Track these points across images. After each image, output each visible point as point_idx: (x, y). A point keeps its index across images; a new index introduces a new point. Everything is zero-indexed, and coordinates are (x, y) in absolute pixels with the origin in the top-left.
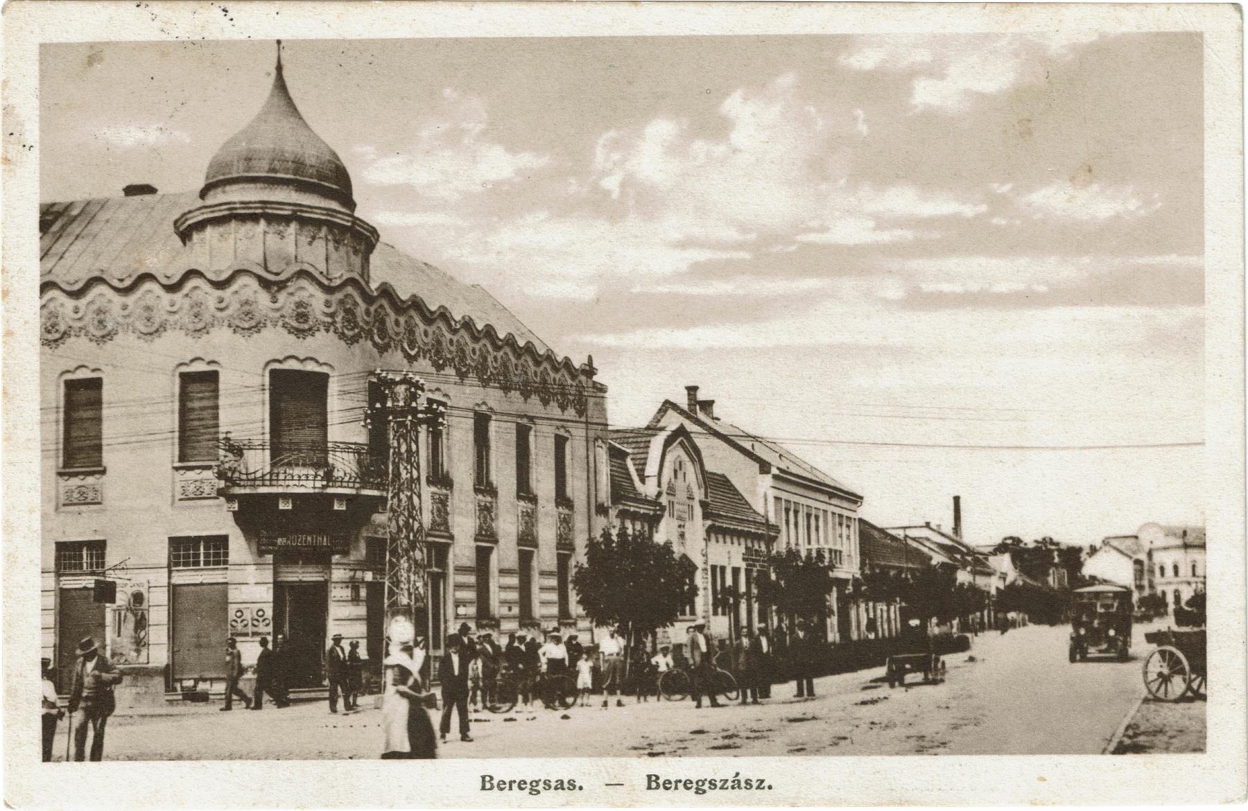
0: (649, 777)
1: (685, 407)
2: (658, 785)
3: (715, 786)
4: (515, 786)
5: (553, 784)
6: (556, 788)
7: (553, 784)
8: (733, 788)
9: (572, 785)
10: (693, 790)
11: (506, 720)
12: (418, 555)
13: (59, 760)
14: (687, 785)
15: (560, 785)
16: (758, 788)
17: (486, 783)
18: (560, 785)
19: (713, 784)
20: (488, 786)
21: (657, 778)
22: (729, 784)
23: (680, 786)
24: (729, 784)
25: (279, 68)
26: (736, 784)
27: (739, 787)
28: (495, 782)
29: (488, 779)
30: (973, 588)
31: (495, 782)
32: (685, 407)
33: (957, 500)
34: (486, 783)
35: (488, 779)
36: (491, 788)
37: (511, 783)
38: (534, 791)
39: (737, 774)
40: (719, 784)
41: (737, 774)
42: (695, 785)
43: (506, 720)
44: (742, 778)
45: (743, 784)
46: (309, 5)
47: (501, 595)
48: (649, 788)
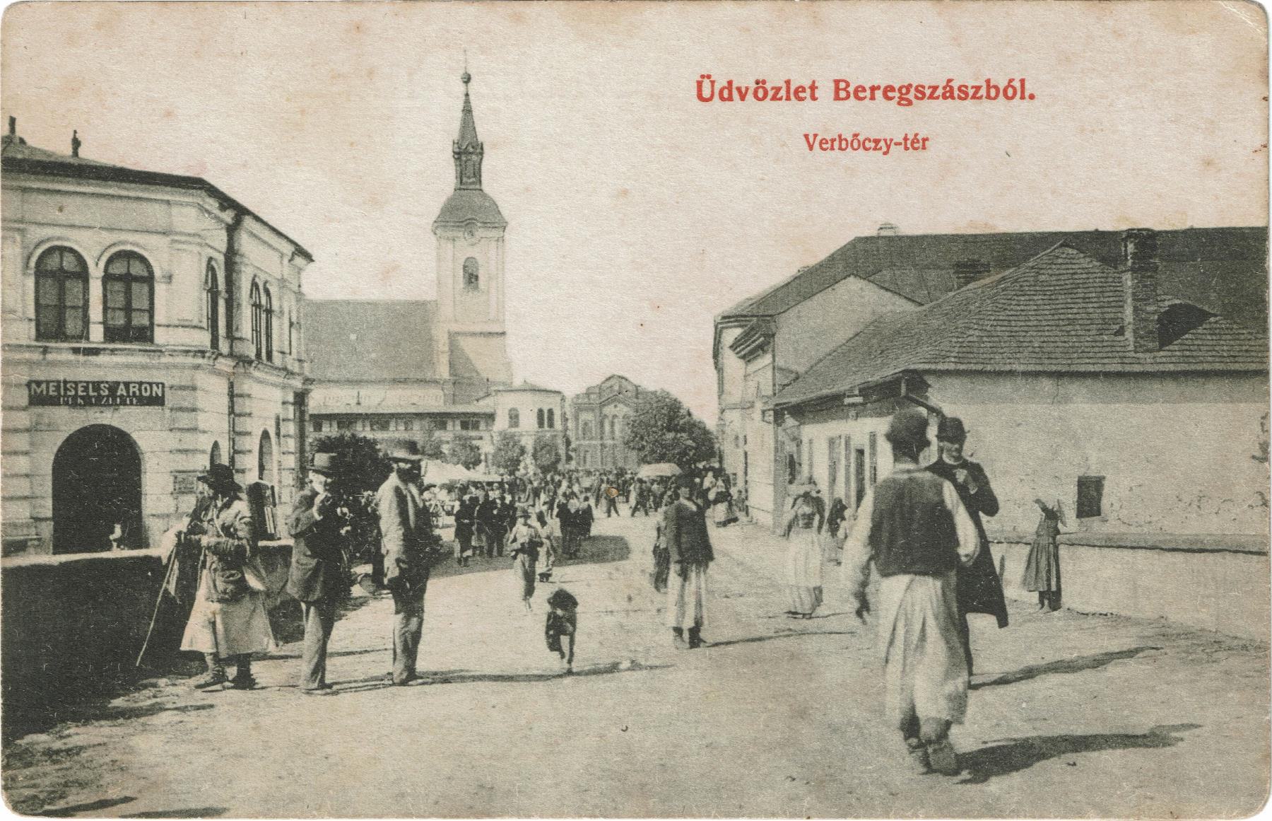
0: (837, 82)
1: (926, 378)
4: (879, 94)
8: (945, 98)
10: (897, 99)
11: (711, 91)
13: (3, 508)
14: (964, 93)
19: (920, 90)
20: (843, 94)
22: (939, 92)
23: (879, 94)
24: (939, 92)
25: (467, 110)
27: (953, 98)
29: (842, 85)
31: (851, 89)
32: (926, 378)
36: (848, 97)
37: (873, 89)
38: (904, 101)
43: (711, 91)
44: (955, 85)
45: (956, 93)
48: (837, 98)
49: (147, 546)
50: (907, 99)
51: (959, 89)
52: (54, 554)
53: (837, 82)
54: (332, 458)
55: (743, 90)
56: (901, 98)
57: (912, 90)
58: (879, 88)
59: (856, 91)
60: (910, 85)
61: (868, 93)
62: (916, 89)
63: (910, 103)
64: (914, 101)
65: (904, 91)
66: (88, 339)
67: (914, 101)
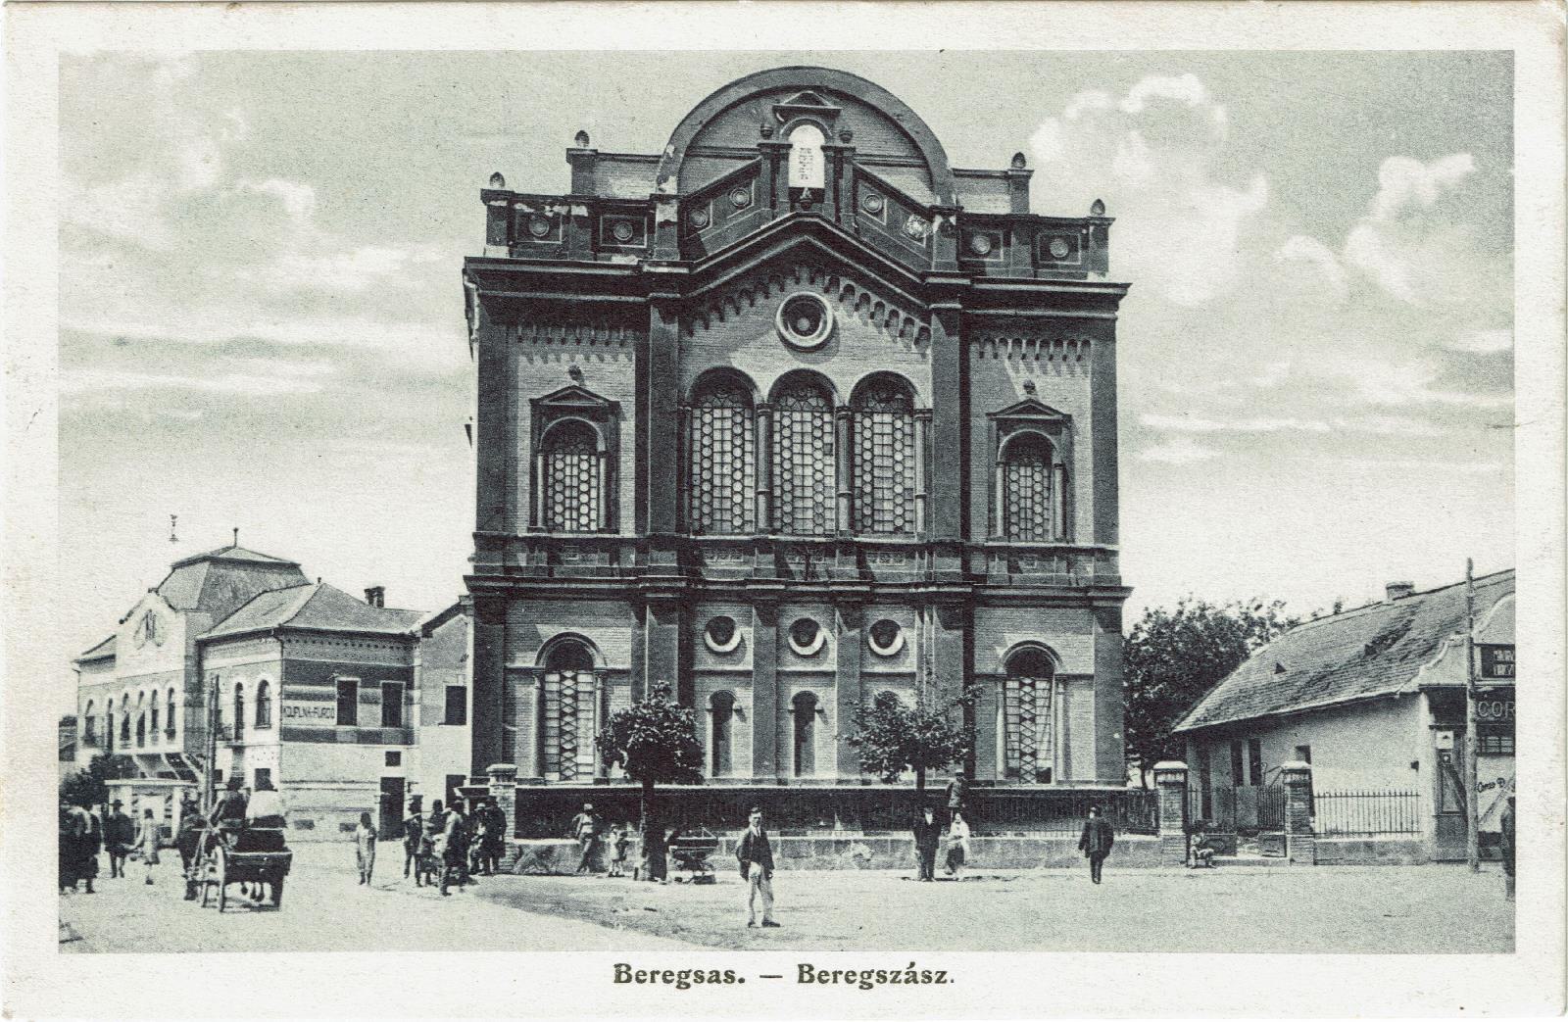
0: (801, 967)
2: (812, 976)
3: (930, 979)
4: (659, 978)
5: (707, 976)
6: (710, 981)
7: (707, 976)
9: (730, 977)
10: (675, 984)
12: (937, 734)
15: (715, 977)
16: (938, 981)
17: (623, 974)
18: (715, 977)
19: (882, 977)
20: (806, 977)
21: (811, 968)
22: (903, 977)
23: (659, 978)
24: (903, 977)
26: (912, 978)
28: (815, 973)
29: (806, 969)
30: (695, 541)
31: (815, 973)
33: (1470, 561)
34: (623, 974)
35: (806, 969)
37: (653, 973)
38: (683, 985)
39: (912, 964)
40: (890, 977)
41: (912, 964)
42: (676, 978)
44: (918, 969)
45: (919, 978)
46: (560, 4)
47: (1333, 807)
48: (618, 980)
49: (463, 689)
50: (685, 983)
51: (726, 974)
52: (402, 779)
53: (801, 967)
54: (95, 758)
55: (66, 935)
56: (679, 982)
57: (692, 975)
58: (658, 972)
59: (637, 974)
60: (873, 971)
61: (831, 977)
62: (696, 973)
63: (871, 986)
64: (875, 984)
65: (683, 975)
66: (1478, 754)
67: (875, 984)
